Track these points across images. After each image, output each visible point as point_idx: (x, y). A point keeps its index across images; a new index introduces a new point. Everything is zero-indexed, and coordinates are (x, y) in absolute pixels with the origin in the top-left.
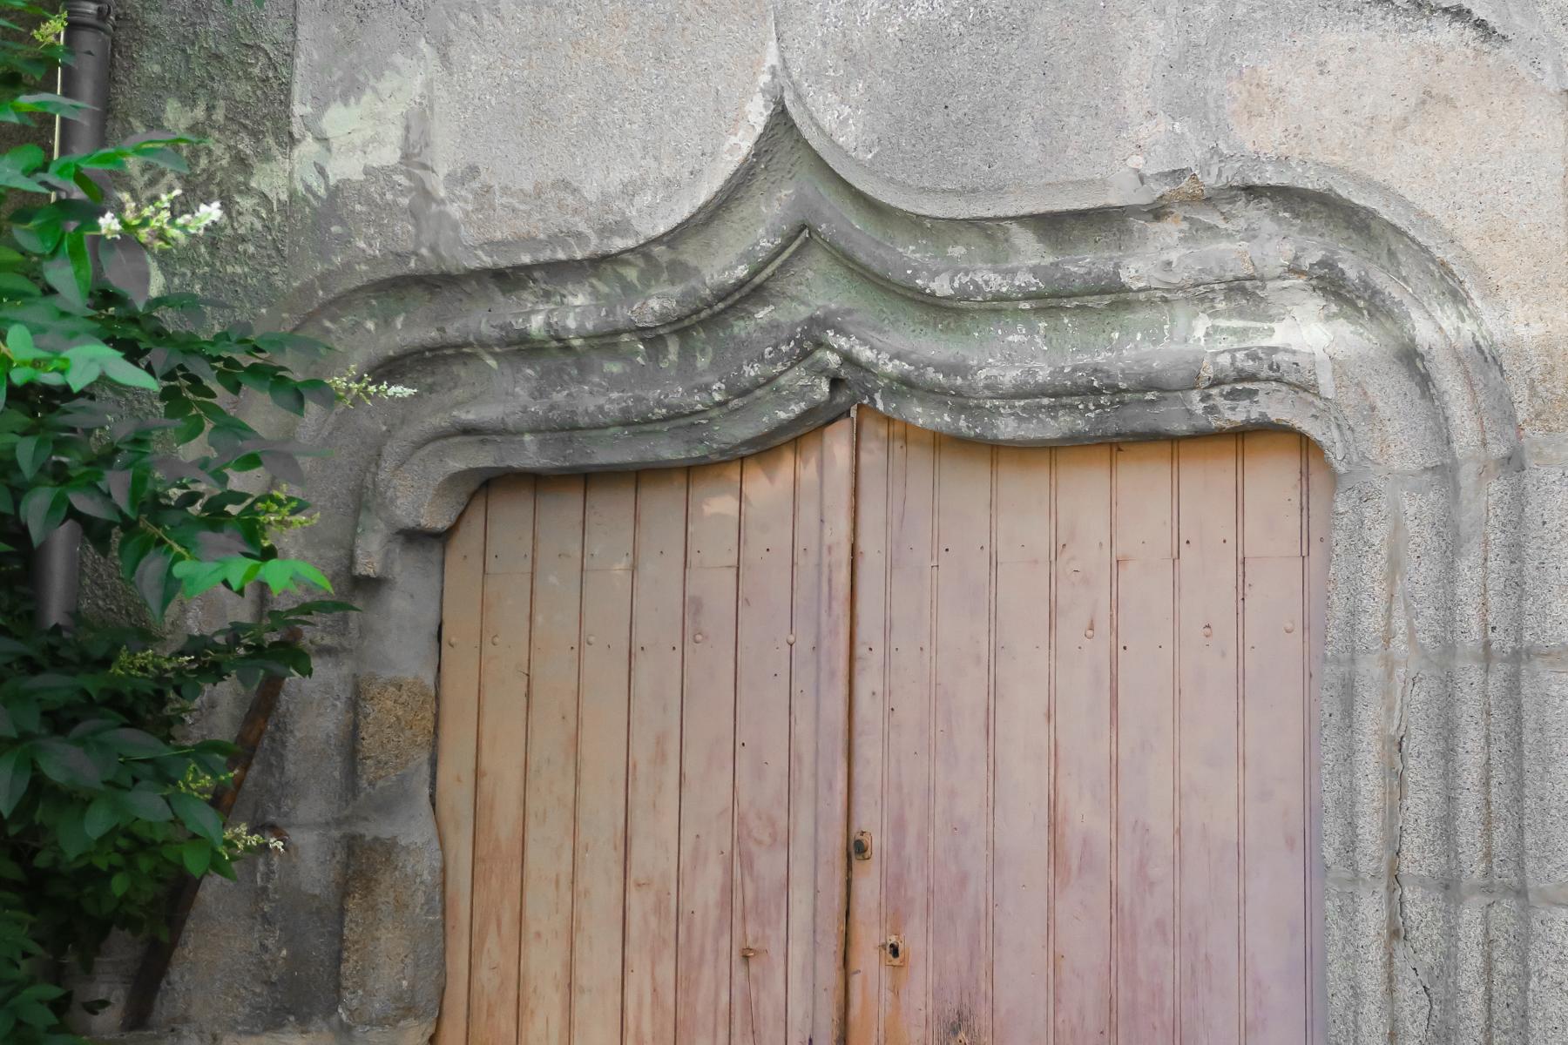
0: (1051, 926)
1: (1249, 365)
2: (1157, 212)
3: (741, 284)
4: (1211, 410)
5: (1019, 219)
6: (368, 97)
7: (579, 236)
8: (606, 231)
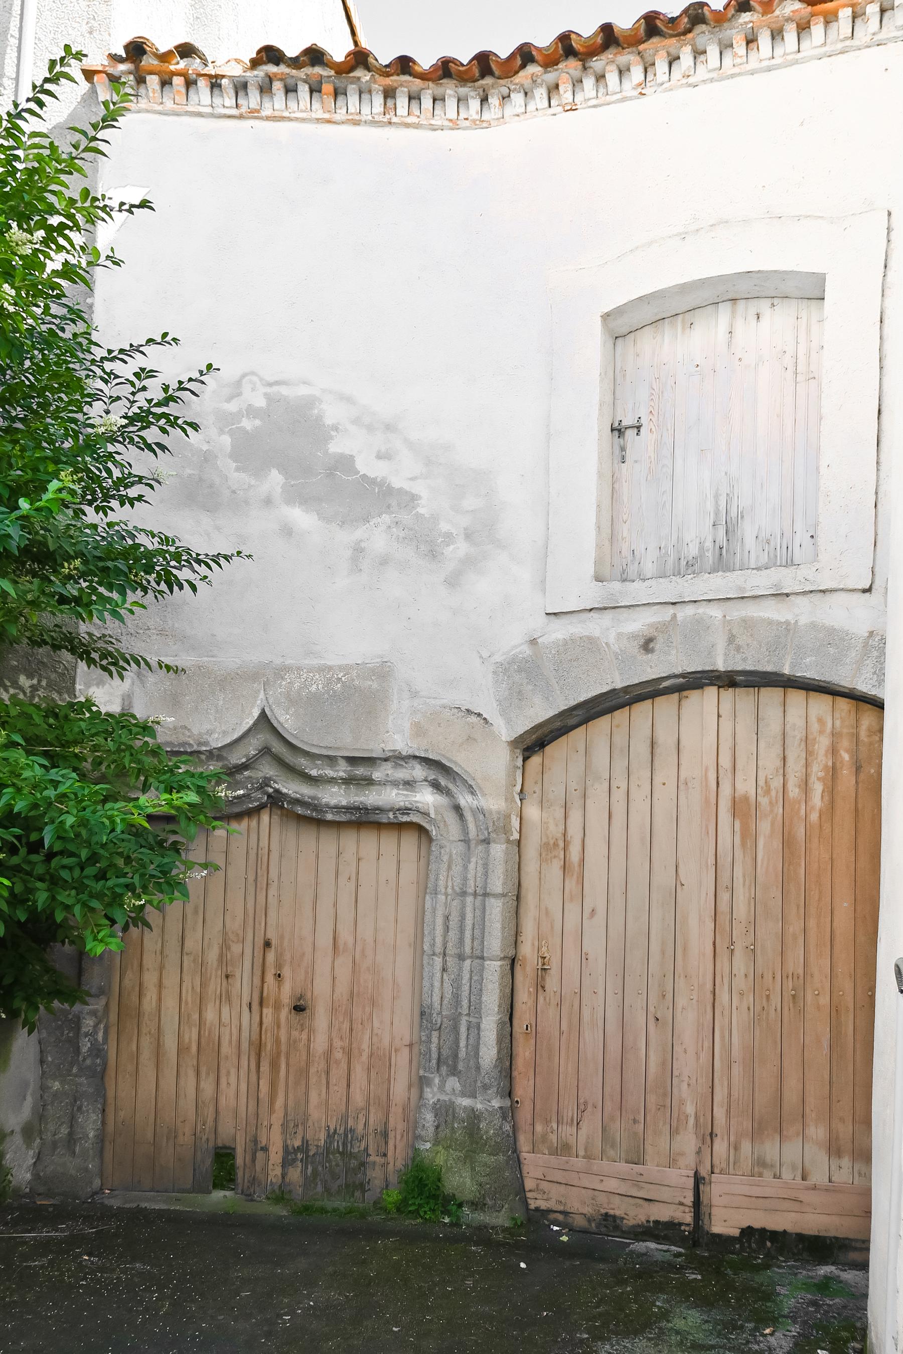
0: (333, 968)
1: (409, 806)
2: (386, 760)
3: (243, 764)
4: (395, 817)
5: (342, 757)
6: (107, 686)
7: (190, 745)
8: (200, 744)
